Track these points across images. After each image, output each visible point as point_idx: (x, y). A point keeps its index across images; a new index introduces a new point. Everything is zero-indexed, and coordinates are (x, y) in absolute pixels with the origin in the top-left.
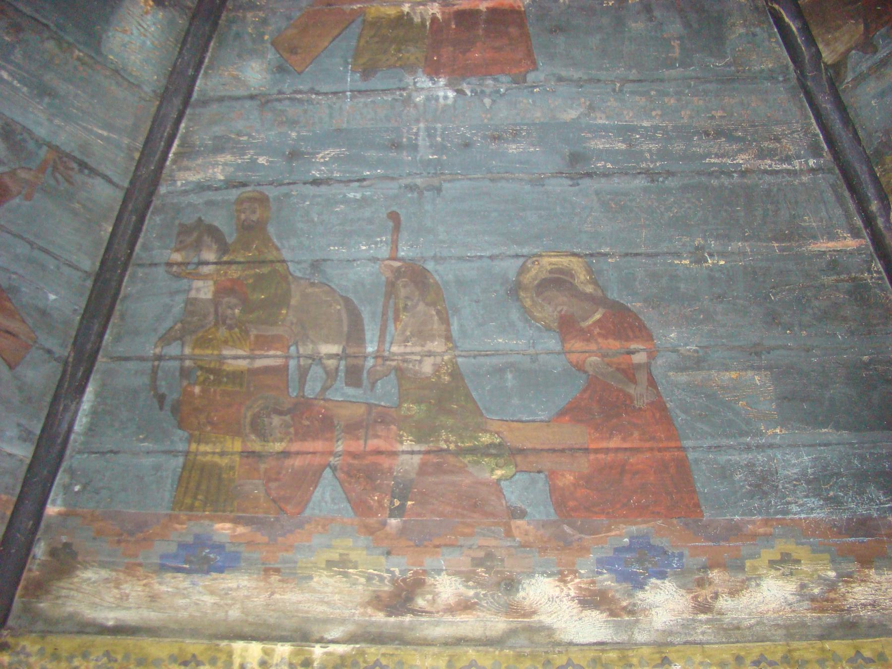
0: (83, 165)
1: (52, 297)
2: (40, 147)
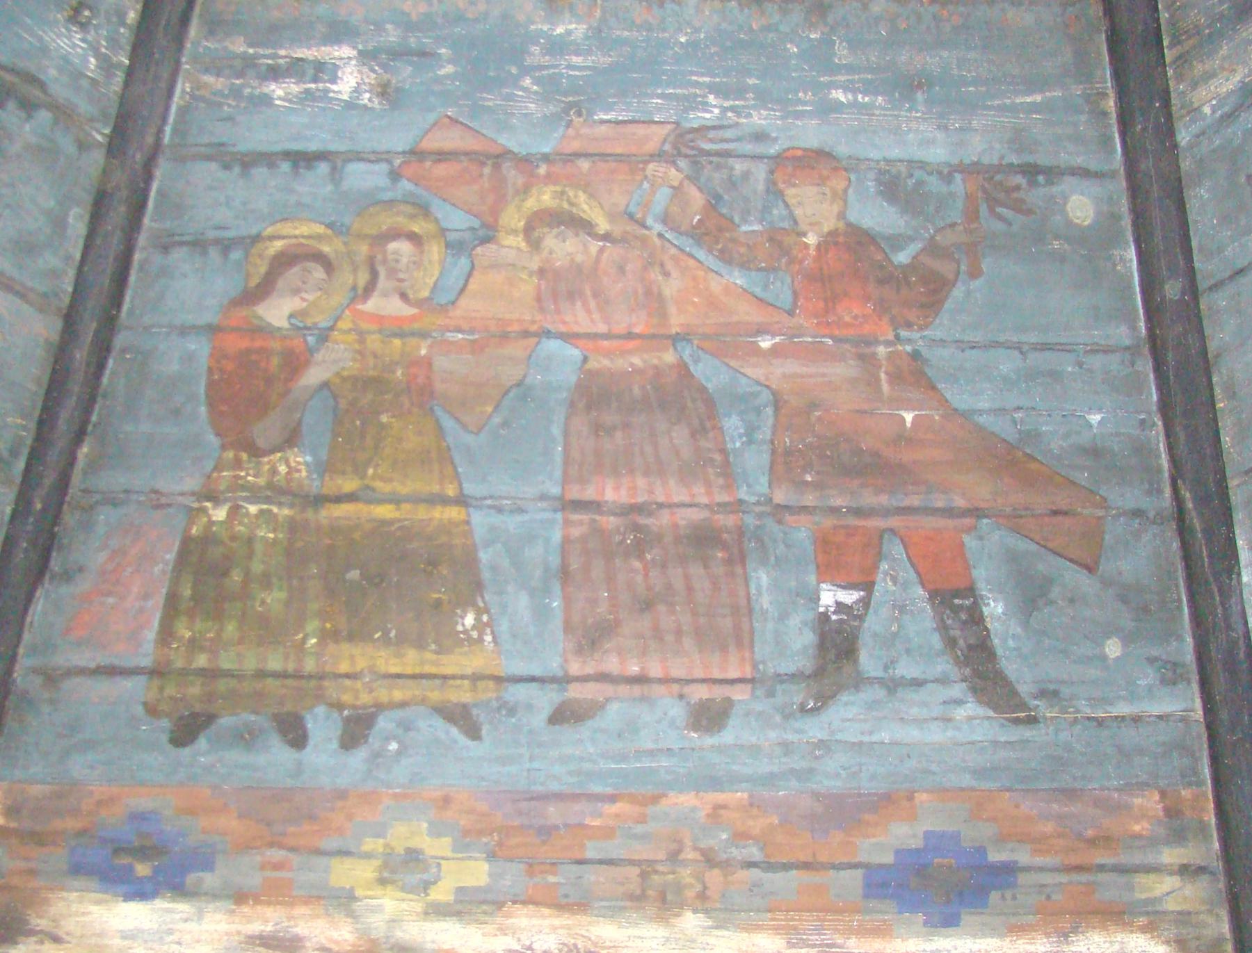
0: (1031, 171)
1: (1095, 418)
2: (947, 178)
